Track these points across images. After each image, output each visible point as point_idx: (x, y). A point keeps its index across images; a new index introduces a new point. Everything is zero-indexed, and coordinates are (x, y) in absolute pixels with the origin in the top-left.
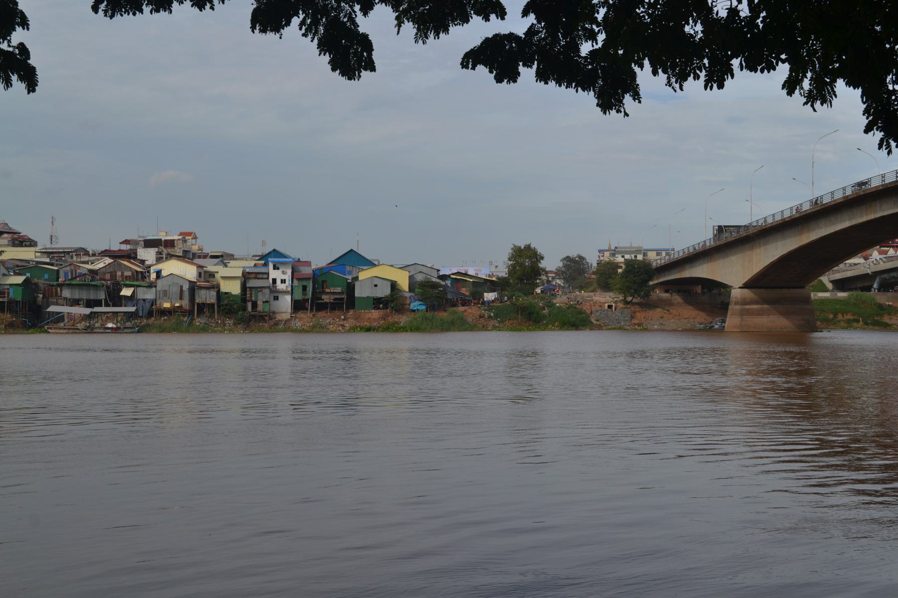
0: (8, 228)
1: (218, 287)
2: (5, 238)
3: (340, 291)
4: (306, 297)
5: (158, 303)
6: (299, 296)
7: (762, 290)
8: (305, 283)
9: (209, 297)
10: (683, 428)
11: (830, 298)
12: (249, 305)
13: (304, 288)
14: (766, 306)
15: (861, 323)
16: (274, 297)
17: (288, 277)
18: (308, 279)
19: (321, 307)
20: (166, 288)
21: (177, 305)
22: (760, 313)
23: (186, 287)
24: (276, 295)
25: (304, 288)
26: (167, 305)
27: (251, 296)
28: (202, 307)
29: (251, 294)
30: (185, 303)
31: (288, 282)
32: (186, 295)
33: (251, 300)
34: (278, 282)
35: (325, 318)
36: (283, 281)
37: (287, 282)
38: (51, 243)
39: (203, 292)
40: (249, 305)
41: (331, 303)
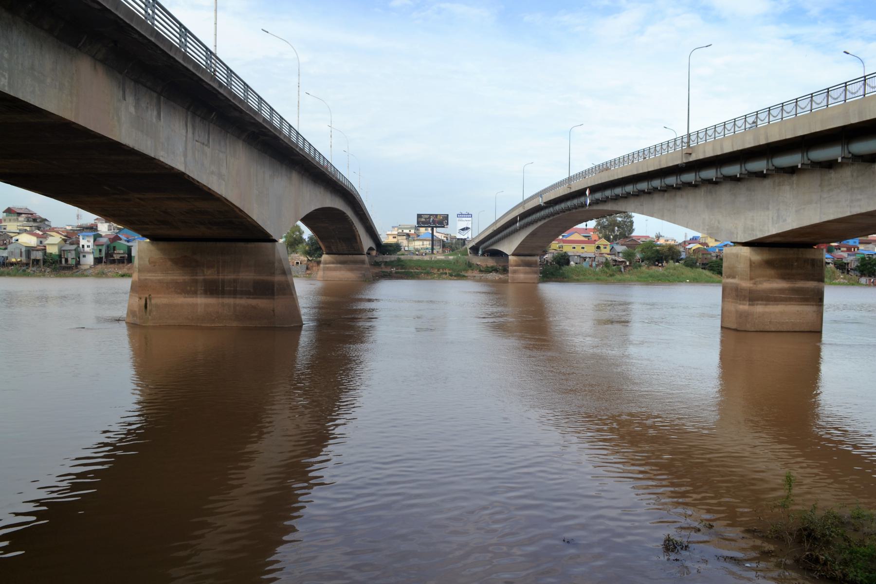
0: (28, 211)
1: (45, 250)
2: (23, 217)
3: (122, 252)
4: (101, 256)
5: (9, 259)
6: (98, 256)
7: (336, 256)
8: (100, 248)
9: (39, 255)
10: (767, 328)
11: (445, 259)
12: (63, 260)
13: (100, 251)
14: (339, 265)
15: (448, 275)
16: (83, 256)
17: (91, 243)
18: (103, 245)
19: (113, 262)
20: (13, 250)
21: (19, 260)
22: (335, 269)
23: (23, 250)
24: (84, 254)
25: (100, 251)
26: (14, 260)
27: (64, 255)
28: (36, 262)
29: (64, 254)
30: (24, 259)
31: (91, 247)
32: (24, 254)
33: (64, 257)
34: (86, 247)
35: (111, 268)
36: (88, 246)
37: (91, 247)
38: (78, 219)
39: (35, 252)
40: (63, 260)
41: (118, 260)
